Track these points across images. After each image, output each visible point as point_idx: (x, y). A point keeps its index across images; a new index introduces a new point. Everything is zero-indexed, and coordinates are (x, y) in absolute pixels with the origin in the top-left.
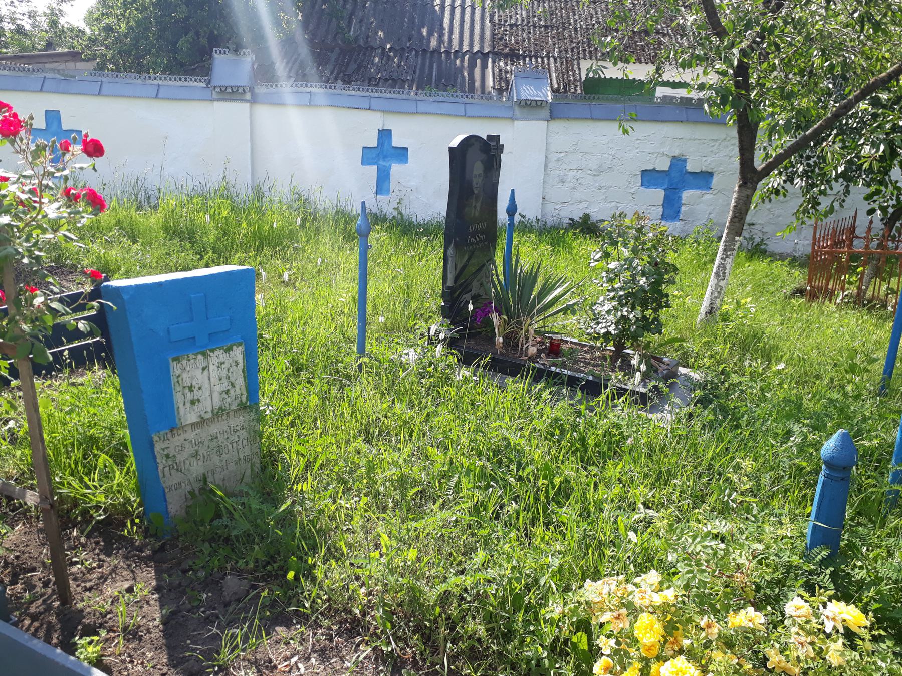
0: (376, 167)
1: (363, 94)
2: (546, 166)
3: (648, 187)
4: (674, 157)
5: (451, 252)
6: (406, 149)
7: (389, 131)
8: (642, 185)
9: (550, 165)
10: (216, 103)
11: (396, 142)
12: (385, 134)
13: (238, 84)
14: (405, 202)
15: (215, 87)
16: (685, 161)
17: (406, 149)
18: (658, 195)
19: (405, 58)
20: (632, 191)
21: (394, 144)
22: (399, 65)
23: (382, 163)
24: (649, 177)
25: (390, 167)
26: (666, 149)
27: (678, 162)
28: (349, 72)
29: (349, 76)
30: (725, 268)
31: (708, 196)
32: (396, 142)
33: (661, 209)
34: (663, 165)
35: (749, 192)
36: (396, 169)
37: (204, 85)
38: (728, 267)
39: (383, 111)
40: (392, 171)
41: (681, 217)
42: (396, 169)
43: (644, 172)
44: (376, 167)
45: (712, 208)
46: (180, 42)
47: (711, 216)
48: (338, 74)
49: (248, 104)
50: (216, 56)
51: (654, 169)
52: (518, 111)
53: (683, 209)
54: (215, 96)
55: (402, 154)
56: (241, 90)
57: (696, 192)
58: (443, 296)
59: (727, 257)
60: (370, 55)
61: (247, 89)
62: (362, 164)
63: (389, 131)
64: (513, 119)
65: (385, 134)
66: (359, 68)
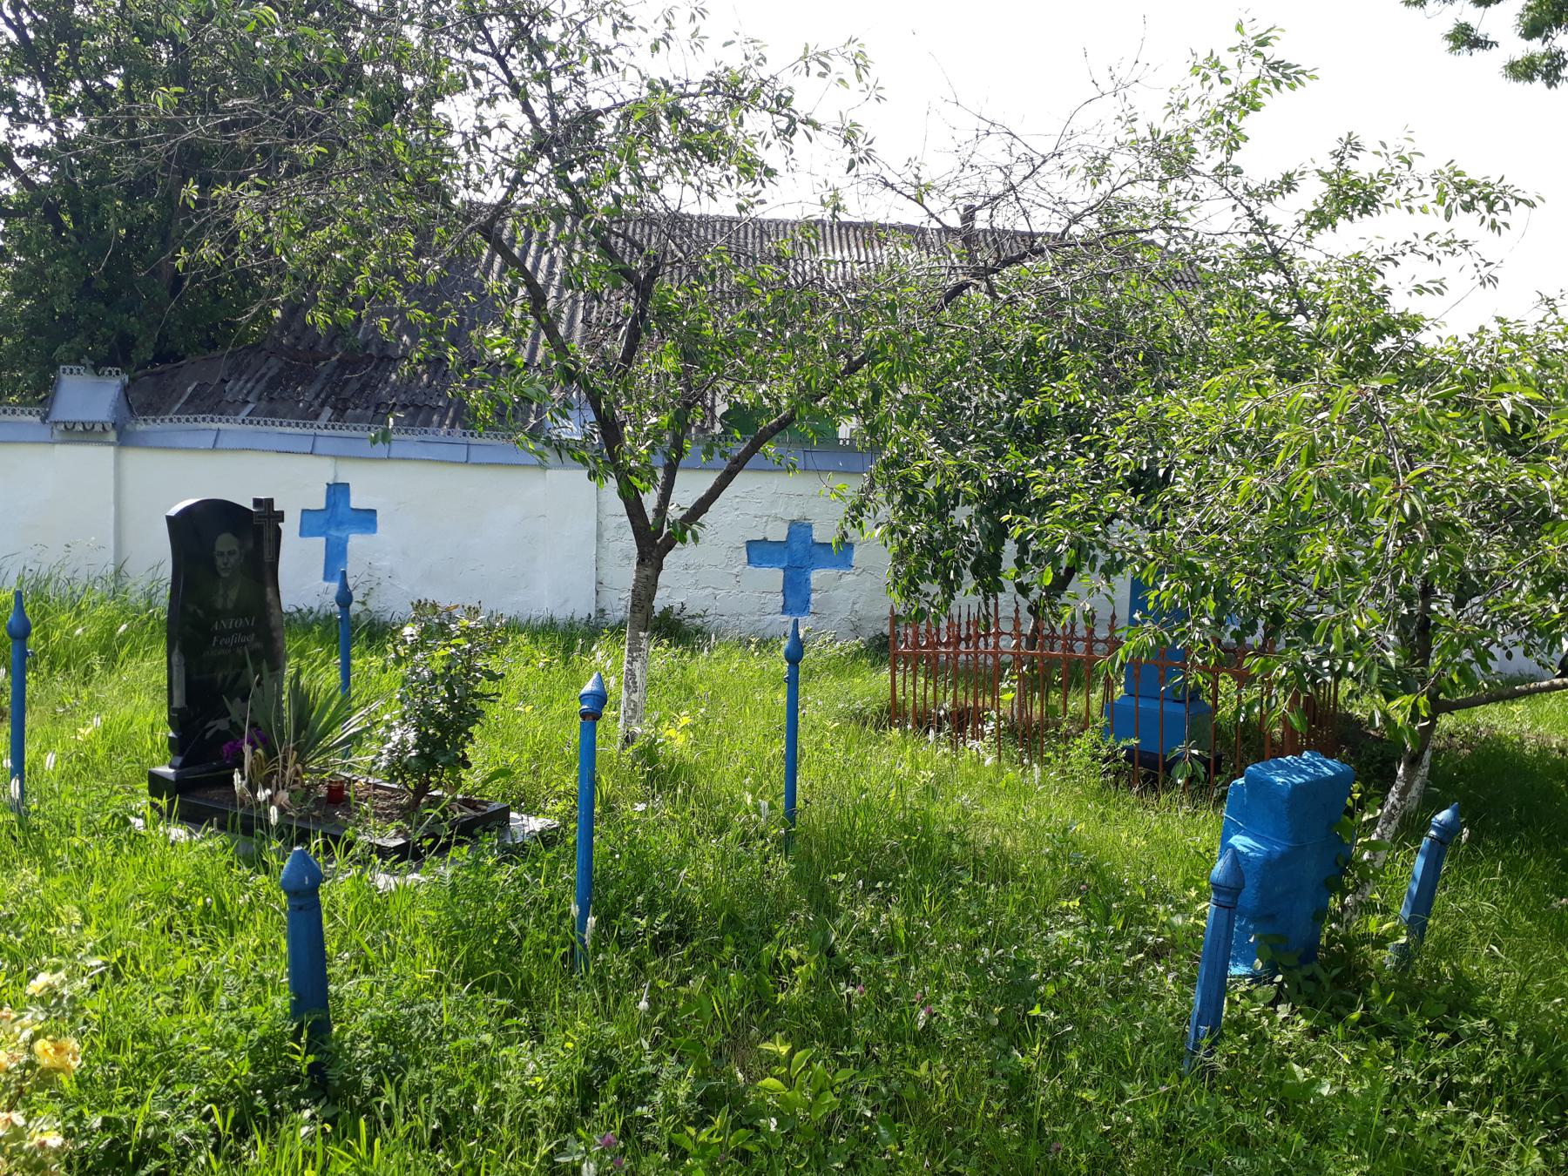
0: (322, 540)
1: (304, 431)
2: (599, 536)
3: (759, 565)
4: (793, 522)
5: (175, 659)
6: (374, 512)
7: (345, 487)
8: (749, 562)
9: (607, 535)
10: (58, 447)
11: (357, 501)
12: (338, 491)
13: (73, 418)
14: (374, 594)
15: (56, 423)
16: (810, 527)
17: (374, 512)
18: (774, 577)
19: (440, 374)
20: (735, 571)
21: (353, 505)
22: (429, 385)
23: (334, 533)
24: (758, 551)
25: (346, 541)
26: (779, 510)
27: (800, 528)
28: (346, 394)
29: (345, 400)
30: (634, 676)
31: (849, 578)
32: (357, 501)
33: (781, 598)
34: (779, 533)
35: (649, 572)
36: (356, 542)
37: (38, 419)
38: (638, 673)
39: (336, 457)
40: (350, 546)
41: (812, 609)
42: (356, 542)
43: (750, 544)
44: (322, 540)
45: (856, 594)
46: (58, 350)
47: (857, 607)
48: (328, 397)
49: (111, 449)
50: (64, 377)
51: (765, 540)
52: (551, 456)
53: (813, 596)
54: (57, 436)
55: (367, 519)
56: (98, 428)
57: (833, 572)
58: (171, 722)
59: (634, 659)
60: (386, 370)
61: (109, 427)
62: (301, 534)
63: (345, 487)
64: (543, 466)
65: (338, 491)
66: (362, 390)
